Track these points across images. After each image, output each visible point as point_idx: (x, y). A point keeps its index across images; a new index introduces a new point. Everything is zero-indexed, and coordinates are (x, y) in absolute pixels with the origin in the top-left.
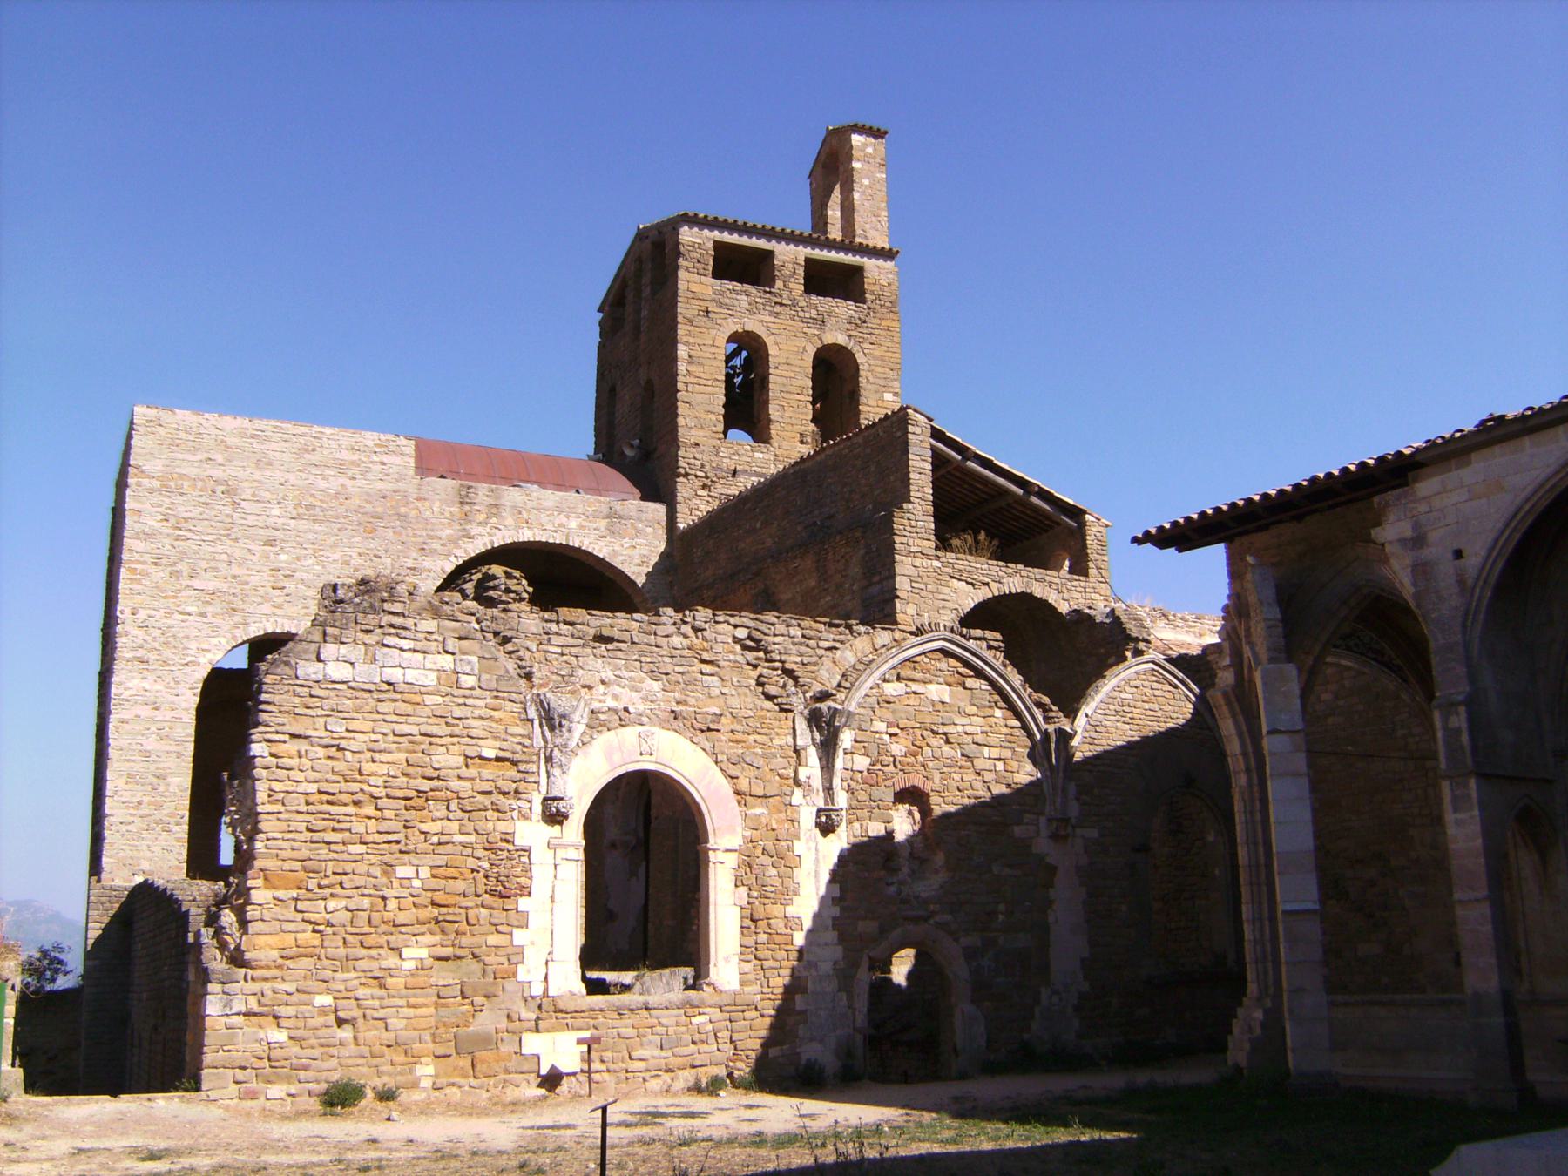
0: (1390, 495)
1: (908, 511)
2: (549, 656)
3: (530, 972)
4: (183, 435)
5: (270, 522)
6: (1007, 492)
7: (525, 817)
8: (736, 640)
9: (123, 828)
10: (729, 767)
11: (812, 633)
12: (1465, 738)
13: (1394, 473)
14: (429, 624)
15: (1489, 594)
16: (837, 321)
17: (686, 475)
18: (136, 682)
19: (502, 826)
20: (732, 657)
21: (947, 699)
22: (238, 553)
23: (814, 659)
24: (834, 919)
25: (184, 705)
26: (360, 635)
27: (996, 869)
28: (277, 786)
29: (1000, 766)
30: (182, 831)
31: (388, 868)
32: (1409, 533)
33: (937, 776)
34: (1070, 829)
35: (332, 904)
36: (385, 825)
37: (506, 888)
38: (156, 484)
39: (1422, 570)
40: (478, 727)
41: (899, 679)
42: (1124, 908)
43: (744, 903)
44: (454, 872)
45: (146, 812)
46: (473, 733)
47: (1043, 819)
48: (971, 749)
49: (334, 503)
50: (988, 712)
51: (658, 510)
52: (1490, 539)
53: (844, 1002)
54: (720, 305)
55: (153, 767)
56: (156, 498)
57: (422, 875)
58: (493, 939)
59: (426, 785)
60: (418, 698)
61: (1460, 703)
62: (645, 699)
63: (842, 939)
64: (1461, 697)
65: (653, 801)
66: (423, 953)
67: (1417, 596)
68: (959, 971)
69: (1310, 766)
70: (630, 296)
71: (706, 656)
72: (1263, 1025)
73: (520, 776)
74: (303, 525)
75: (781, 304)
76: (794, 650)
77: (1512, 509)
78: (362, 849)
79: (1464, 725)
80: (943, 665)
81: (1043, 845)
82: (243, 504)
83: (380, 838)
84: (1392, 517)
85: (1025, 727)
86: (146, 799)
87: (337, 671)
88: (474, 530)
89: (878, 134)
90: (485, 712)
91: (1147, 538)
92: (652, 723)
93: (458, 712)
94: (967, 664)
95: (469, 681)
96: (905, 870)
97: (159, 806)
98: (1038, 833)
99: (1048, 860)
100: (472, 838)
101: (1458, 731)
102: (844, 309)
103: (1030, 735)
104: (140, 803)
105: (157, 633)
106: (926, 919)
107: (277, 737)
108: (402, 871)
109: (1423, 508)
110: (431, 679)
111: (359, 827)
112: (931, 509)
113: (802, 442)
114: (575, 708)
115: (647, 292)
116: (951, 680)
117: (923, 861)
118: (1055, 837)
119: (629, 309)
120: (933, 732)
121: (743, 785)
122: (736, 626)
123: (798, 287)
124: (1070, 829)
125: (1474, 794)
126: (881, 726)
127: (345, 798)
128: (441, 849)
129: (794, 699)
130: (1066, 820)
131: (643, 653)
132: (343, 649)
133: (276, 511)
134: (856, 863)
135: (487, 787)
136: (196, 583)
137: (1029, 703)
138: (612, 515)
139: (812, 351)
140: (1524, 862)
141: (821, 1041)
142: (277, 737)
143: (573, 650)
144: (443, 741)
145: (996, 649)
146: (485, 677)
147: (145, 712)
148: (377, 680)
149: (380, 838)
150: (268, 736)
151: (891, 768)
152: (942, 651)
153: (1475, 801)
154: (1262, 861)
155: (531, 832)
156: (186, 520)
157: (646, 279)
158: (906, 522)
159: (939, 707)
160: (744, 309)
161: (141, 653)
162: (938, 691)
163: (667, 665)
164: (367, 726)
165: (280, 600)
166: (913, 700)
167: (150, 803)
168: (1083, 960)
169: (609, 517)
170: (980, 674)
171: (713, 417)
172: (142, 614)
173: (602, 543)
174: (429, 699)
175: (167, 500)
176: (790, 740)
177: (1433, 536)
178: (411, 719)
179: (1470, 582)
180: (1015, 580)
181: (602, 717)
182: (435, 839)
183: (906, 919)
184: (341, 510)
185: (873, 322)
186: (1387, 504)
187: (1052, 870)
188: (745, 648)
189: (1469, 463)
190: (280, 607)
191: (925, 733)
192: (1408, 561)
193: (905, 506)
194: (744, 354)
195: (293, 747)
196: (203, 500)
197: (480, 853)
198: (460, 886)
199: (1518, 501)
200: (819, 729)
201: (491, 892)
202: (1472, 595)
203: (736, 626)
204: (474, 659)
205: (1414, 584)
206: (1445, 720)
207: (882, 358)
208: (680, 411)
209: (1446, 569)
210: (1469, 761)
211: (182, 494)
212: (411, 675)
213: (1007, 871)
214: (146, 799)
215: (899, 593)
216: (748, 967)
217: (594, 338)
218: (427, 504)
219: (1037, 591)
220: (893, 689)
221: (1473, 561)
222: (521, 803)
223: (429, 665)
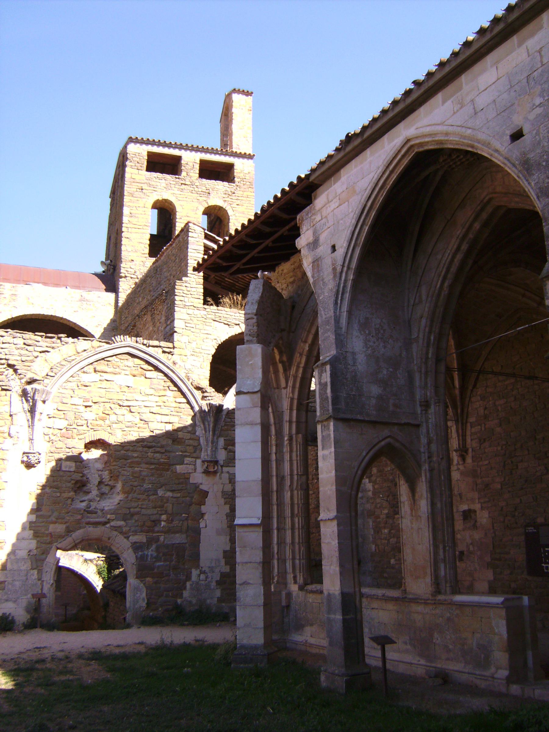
1: (186, 282)
11: (29, 342)
15: (351, 277)
16: (217, 193)
17: (126, 277)
27: (160, 493)
47: (199, 462)
48: (147, 416)
51: (112, 296)
53: (36, 576)
54: (150, 185)
63: (36, 535)
68: (129, 558)
75: (185, 184)
76: (17, 352)
81: (198, 477)
85: (189, 402)
89: (248, 94)
98: (195, 470)
99: (202, 487)
102: (220, 186)
103: (192, 408)
106: (105, 523)
116: (135, 373)
118: (206, 472)
129: (12, 383)
130: (216, 462)
134: (51, 487)
137: (191, 387)
141: (15, 602)
151: (85, 427)
152: (128, 354)
153: (332, 439)
158: (184, 288)
159: (126, 389)
160: (163, 187)
168: (225, 552)
169: (81, 300)
170: (157, 369)
176: (7, 408)
179: (339, 269)
185: (239, 193)
187: (205, 494)
191: (113, 406)
193: (184, 279)
200: (27, 401)
202: (340, 279)
208: (123, 243)
213: (169, 494)
215: (176, 329)
221: (340, 252)
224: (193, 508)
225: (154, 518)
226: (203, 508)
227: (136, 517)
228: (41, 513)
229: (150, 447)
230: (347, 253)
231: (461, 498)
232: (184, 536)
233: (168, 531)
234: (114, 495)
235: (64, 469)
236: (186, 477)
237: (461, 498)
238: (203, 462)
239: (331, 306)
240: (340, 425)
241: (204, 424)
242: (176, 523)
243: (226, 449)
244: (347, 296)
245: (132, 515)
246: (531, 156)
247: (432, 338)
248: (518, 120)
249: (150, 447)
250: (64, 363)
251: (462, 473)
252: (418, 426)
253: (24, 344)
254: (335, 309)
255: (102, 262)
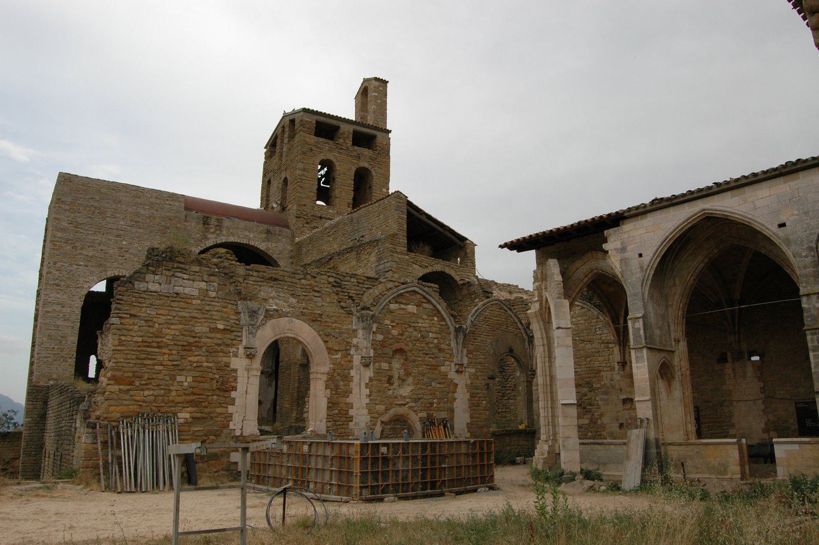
0: (611, 231)
2: (249, 285)
3: (235, 425)
4: (81, 187)
5: (119, 227)
6: (436, 230)
7: (236, 356)
8: (329, 283)
9: (45, 359)
10: (326, 337)
12: (642, 332)
13: (616, 220)
14: (197, 269)
18: (53, 294)
19: (225, 359)
20: (327, 290)
21: (415, 312)
22: (104, 240)
23: (362, 292)
24: (367, 404)
25: (76, 306)
26: (164, 271)
27: (433, 384)
28: (123, 338)
29: (436, 341)
30: (72, 361)
31: (173, 378)
32: (619, 246)
33: (410, 345)
34: (464, 369)
35: (146, 393)
36: (172, 358)
37: (225, 386)
38: (68, 207)
39: (624, 261)
40: (216, 315)
41: (396, 302)
42: (484, 402)
43: (329, 396)
44: (203, 380)
45: (56, 352)
46: (214, 317)
47: (453, 364)
49: (148, 221)
50: (431, 318)
52: (655, 249)
55: (60, 333)
56: (67, 214)
57: (188, 380)
58: (219, 410)
59: (191, 340)
60: (189, 301)
61: (640, 318)
62: (289, 306)
64: (640, 315)
65: (281, 355)
66: (188, 416)
67: (622, 273)
69: (573, 344)
70: (279, 141)
71: (316, 289)
72: (548, 452)
73: (233, 337)
74: (134, 230)
77: (664, 237)
78: (161, 368)
79: (642, 327)
80: (414, 297)
81: (452, 375)
82: (107, 218)
83: (169, 363)
84: (612, 239)
86: (56, 347)
87: (153, 287)
88: (210, 236)
90: (220, 308)
91: (506, 245)
92: (292, 316)
93: (207, 308)
94: (425, 297)
95: (213, 294)
96: (396, 384)
97: (62, 350)
99: (455, 381)
100: (211, 365)
101: (639, 329)
102: (366, 152)
104: (54, 348)
105: (65, 273)
106: (404, 405)
107: (124, 316)
108: (179, 378)
109: (626, 236)
110: (196, 293)
111: (160, 358)
112: (406, 234)
113: (348, 207)
114: (259, 308)
115: (286, 140)
117: (403, 380)
118: (457, 372)
119: (278, 147)
120: (410, 326)
121: (330, 345)
122: (329, 276)
123: (349, 142)
124: (464, 369)
125: (645, 356)
126: (388, 322)
127: (155, 345)
128: (198, 369)
129: (353, 309)
130: (462, 365)
131: (289, 286)
132: (157, 277)
133: (122, 223)
135: (219, 342)
136: (84, 252)
138: (268, 232)
139: (354, 169)
140: (661, 385)
142: (124, 316)
143: (259, 283)
144: (200, 321)
145: (436, 291)
146: (220, 293)
147: (58, 308)
148: (171, 292)
149: (169, 363)
150: (120, 315)
154: (548, 383)
155: (238, 363)
156: (81, 224)
157: (286, 135)
161: (57, 282)
162: (412, 308)
163: (299, 292)
164: (166, 312)
165: (122, 262)
166: (402, 312)
167: (58, 348)
168: (467, 424)
171: (312, 194)
172: (59, 264)
173: (263, 244)
174: (194, 302)
175: (72, 215)
177: (629, 248)
178: (187, 310)
179: (645, 267)
180: (438, 266)
181: (271, 313)
182: (195, 364)
183: (396, 405)
184: (151, 224)
186: (610, 235)
188: (333, 286)
189: (647, 217)
190: (122, 264)
191: (406, 326)
192: (619, 258)
194: (326, 169)
195: (131, 321)
196: (89, 215)
197: (215, 371)
198: (206, 385)
199: (667, 234)
201: (219, 389)
203: (329, 276)
204: (216, 284)
205: (621, 268)
206: (633, 324)
207: (382, 174)
209: (635, 262)
210: (643, 341)
211: (79, 213)
212: (187, 290)
213: (438, 385)
214: (56, 347)
216: (329, 424)
217: (262, 159)
218: (189, 223)
219: (447, 270)
220: (393, 306)
221: (647, 258)
222: (234, 349)
223: (195, 286)
224: (450, 395)
225: (430, 401)
226: (456, 395)
227: (422, 400)
228: (371, 398)
229: (427, 354)
230: (652, 260)
231: (621, 391)
232: (446, 413)
233: (439, 410)
234: (405, 386)
235: (382, 368)
236: (445, 376)
237: (621, 391)
238: (455, 364)
239: (639, 287)
240: (648, 350)
241: (457, 340)
242: (442, 405)
243: (467, 356)
244: (649, 282)
245: (419, 399)
246: (791, 237)
247: (681, 305)
248: (783, 219)
249: (427, 354)
250: (380, 296)
251: (622, 376)
252: (673, 352)
253: (357, 282)
254: (642, 288)
255: (476, 245)
